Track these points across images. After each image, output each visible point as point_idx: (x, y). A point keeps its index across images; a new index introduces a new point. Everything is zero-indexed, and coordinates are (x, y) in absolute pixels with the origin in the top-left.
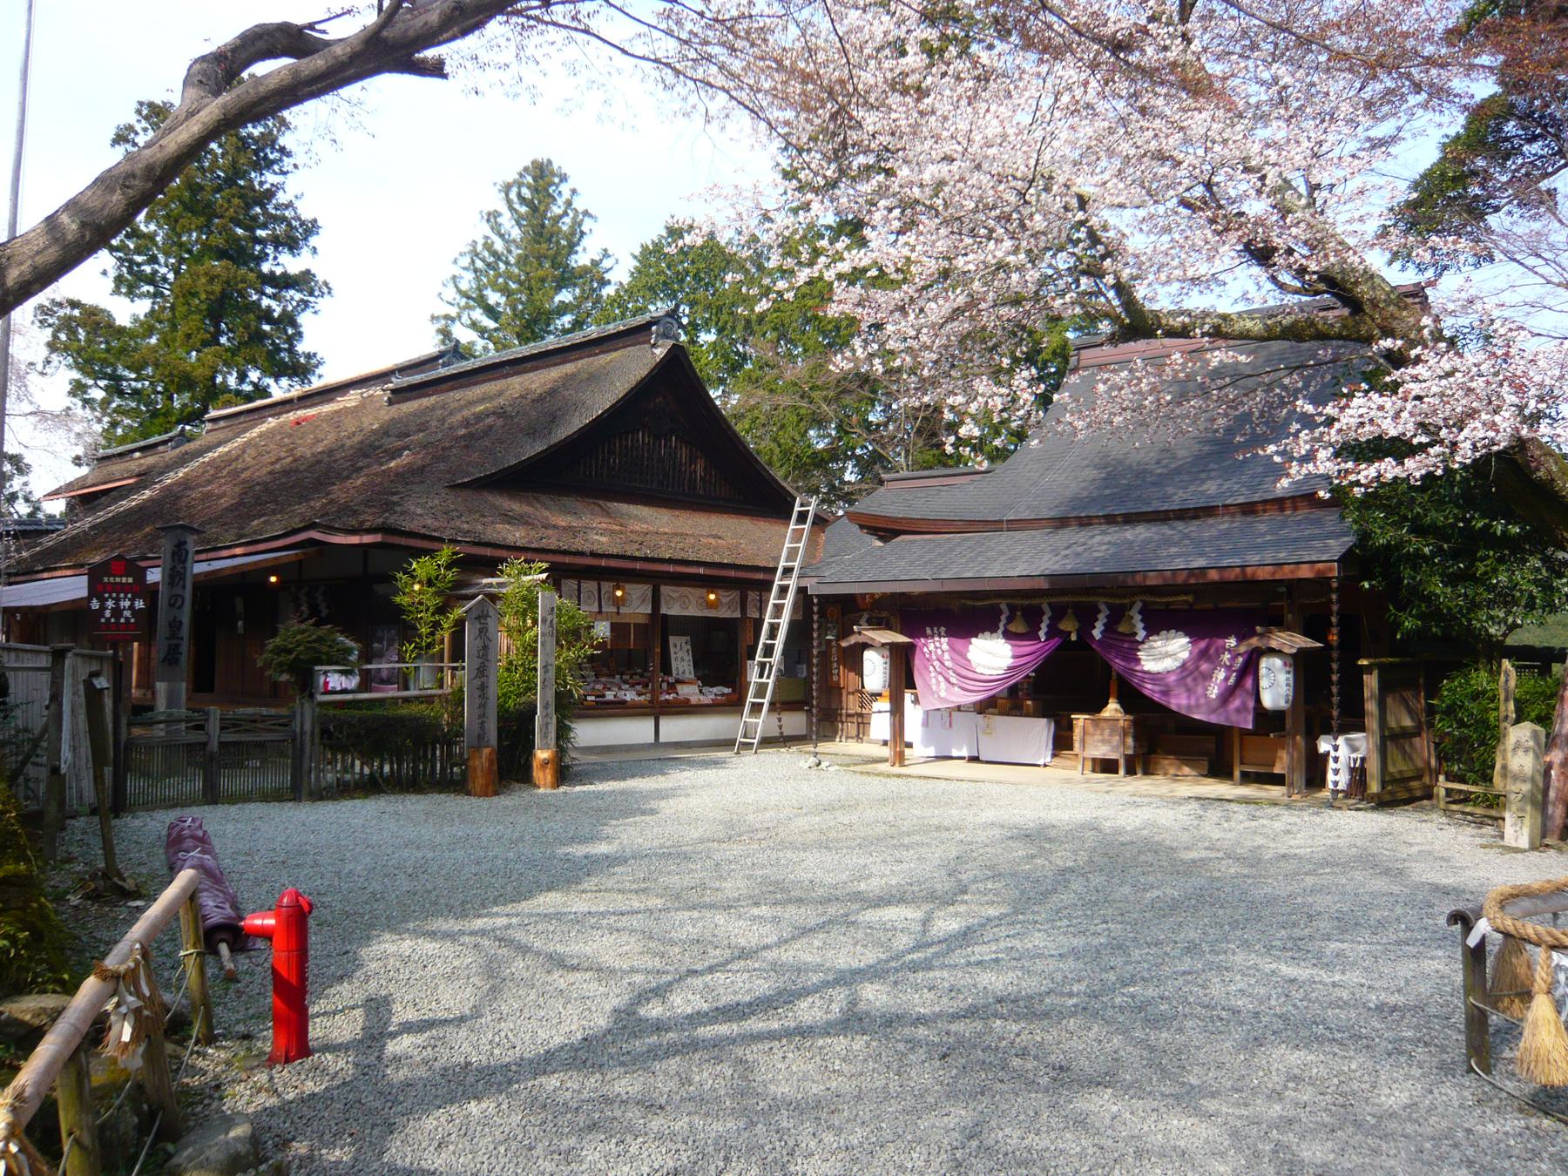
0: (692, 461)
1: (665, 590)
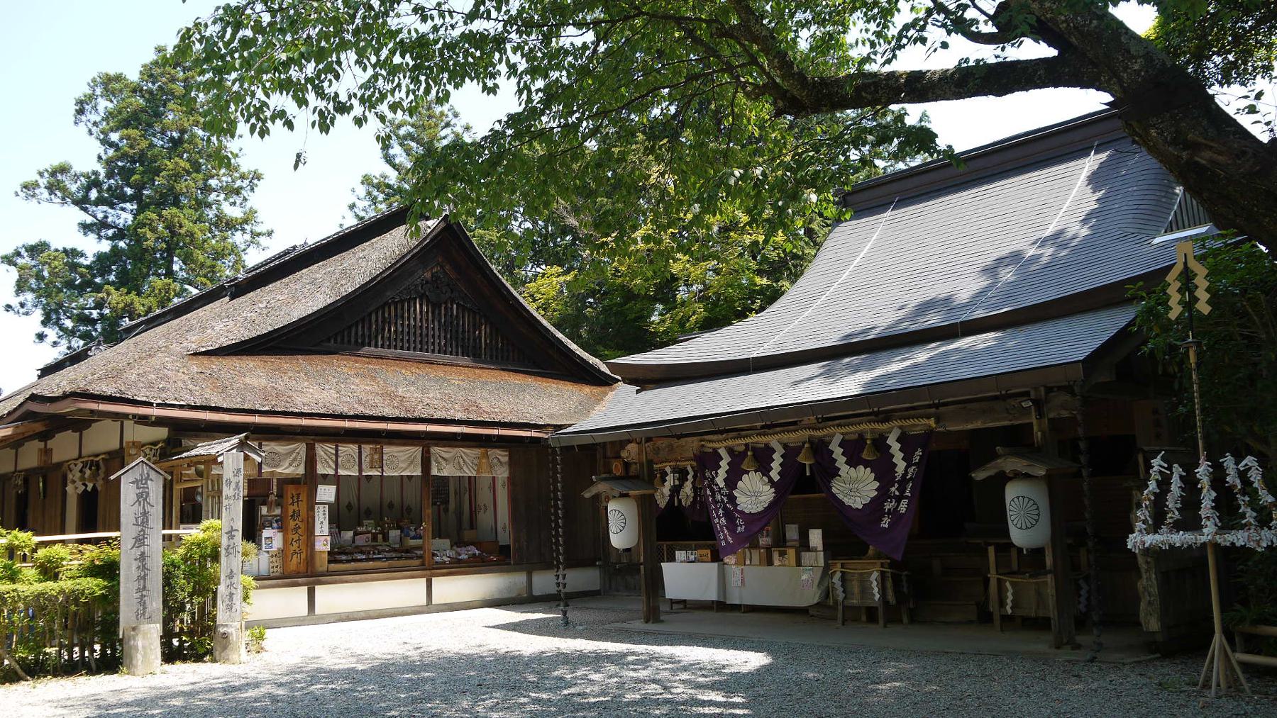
0: (476, 326)
1: (435, 450)
